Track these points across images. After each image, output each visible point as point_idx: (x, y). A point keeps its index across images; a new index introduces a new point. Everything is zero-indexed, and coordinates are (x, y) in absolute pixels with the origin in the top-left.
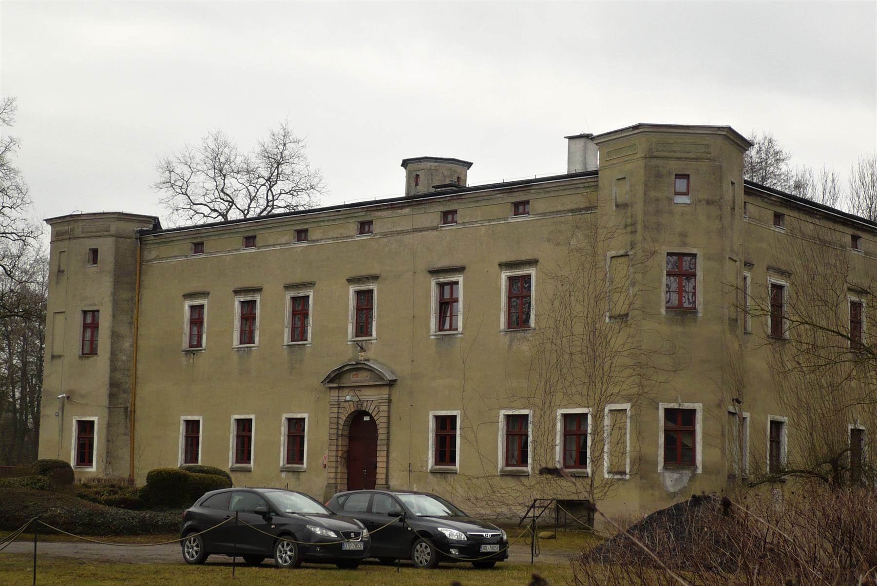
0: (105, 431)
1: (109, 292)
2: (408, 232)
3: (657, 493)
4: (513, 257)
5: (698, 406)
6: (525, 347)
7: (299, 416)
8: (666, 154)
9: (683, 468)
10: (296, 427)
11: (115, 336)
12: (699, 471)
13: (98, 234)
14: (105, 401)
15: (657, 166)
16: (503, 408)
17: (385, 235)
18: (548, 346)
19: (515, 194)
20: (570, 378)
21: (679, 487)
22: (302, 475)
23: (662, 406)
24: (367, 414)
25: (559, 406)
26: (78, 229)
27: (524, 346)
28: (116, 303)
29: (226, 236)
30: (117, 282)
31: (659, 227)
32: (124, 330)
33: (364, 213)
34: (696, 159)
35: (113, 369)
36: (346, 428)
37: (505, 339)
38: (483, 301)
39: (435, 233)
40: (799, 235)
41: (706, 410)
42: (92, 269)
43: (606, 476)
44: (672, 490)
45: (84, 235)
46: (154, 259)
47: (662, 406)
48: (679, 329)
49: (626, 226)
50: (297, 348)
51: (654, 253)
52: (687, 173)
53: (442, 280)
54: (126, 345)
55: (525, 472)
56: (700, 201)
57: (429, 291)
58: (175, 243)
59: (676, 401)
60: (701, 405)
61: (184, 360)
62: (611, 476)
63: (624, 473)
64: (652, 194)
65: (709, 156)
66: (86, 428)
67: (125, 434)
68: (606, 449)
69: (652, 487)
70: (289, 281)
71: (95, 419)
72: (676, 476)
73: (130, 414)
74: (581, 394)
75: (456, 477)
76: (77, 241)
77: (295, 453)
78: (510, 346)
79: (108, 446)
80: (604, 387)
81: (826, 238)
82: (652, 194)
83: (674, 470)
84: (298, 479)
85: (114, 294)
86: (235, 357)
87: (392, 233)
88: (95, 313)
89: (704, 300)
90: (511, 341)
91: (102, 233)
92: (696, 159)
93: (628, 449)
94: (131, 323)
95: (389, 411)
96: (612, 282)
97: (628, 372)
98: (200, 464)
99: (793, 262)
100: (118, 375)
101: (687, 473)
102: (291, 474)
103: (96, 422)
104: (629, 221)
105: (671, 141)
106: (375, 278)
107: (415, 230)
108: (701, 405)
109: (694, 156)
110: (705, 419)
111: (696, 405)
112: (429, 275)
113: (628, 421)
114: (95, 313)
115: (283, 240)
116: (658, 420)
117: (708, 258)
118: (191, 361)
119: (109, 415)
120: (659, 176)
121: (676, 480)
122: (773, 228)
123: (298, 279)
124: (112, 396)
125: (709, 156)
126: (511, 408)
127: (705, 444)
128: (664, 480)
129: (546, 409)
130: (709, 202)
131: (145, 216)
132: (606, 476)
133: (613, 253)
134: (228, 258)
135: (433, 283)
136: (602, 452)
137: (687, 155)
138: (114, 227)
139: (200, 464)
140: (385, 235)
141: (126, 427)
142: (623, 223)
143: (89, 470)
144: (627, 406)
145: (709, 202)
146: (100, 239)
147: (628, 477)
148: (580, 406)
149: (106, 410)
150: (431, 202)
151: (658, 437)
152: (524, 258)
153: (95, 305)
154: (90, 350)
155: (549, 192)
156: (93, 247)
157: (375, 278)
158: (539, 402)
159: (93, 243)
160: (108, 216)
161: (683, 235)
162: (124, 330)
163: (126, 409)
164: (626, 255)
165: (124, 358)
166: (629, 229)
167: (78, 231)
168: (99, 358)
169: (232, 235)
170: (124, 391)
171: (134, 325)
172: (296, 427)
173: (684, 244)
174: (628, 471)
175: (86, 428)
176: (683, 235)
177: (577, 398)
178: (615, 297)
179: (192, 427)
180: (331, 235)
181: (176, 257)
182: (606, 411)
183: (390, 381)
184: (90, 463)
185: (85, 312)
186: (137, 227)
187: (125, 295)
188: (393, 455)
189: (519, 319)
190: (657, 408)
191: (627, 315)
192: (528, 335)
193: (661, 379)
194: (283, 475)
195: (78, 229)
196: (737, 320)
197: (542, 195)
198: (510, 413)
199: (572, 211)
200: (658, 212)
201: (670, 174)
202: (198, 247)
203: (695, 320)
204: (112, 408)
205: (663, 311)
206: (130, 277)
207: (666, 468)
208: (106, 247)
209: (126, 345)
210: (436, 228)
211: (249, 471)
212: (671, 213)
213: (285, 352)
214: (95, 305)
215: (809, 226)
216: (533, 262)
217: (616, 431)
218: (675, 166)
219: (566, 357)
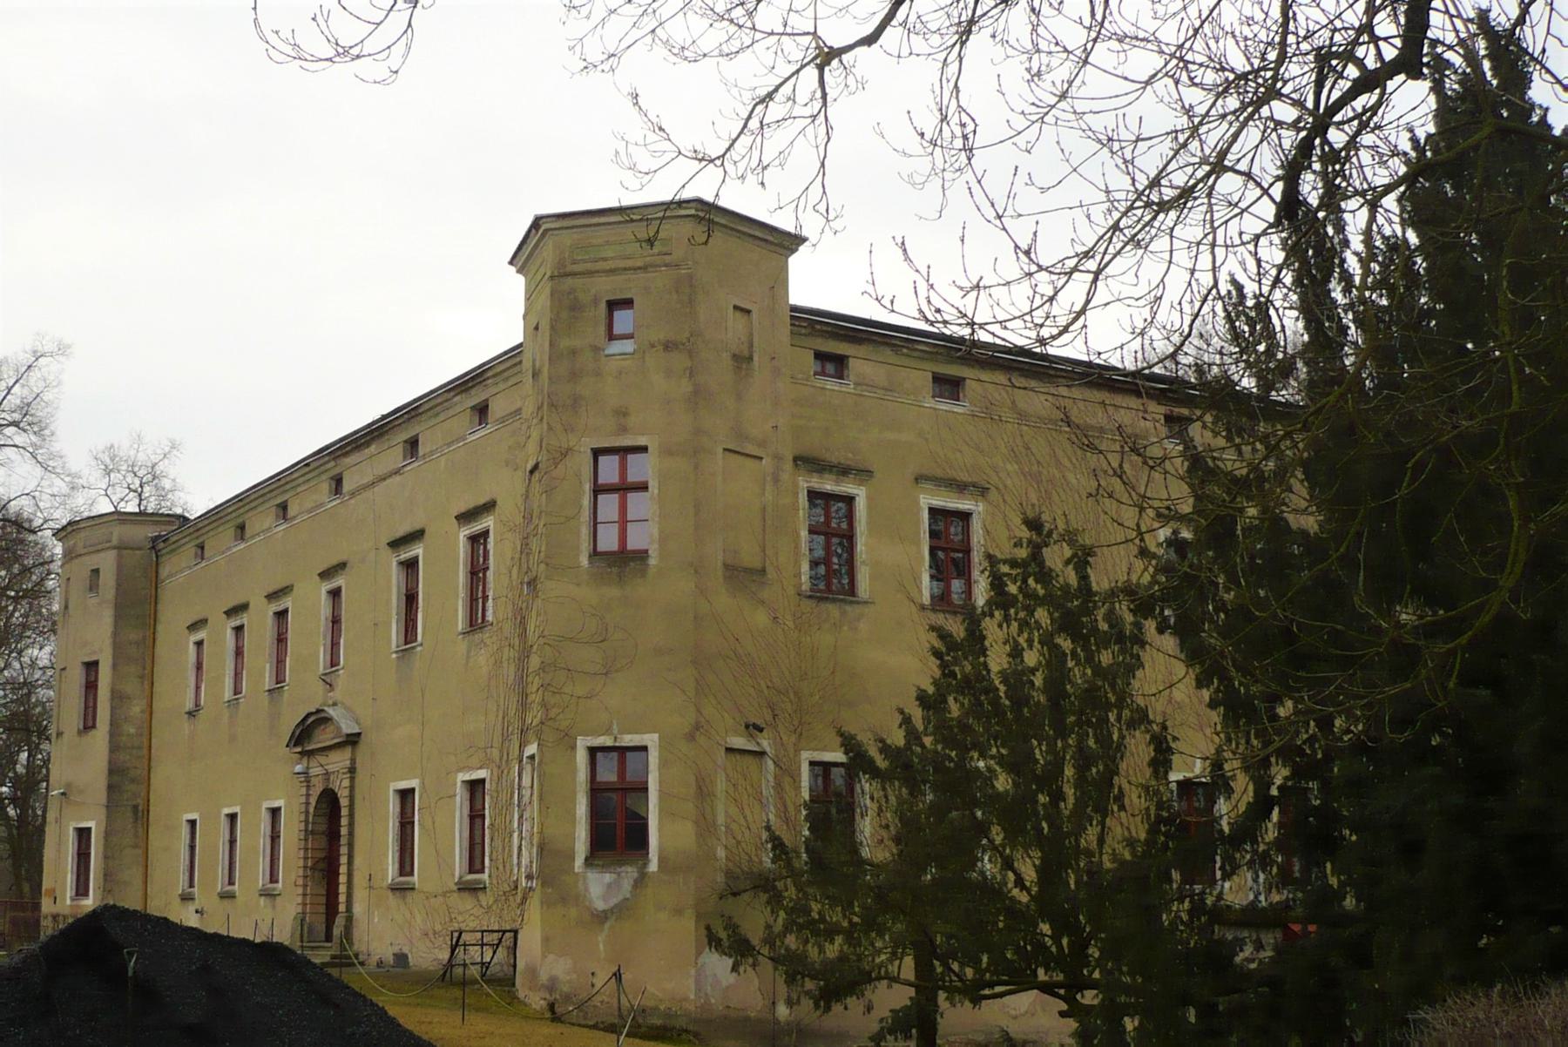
0: (102, 842)
3: (573, 912)
8: (589, 266)
9: (621, 863)
11: (118, 697)
12: (653, 866)
14: (101, 796)
15: (572, 291)
16: (460, 770)
19: (473, 392)
21: (614, 901)
23: (582, 743)
24: (831, 810)
28: (118, 647)
30: (119, 617)
31: (576, 402)
32: (131, 687)
33: (332, 464)
34: (644, 268)
35: (114, 748)
36: (319, 820)
37: (462, 646)
39: (397, 478)
40: (1007, 415)
41: (665, 746)
42: (93, 601)
44: (600, 905)
47: (582, 743)
48: (613, 592)
51: (566, 453)
52: (629, 296)
54: (136, 709)
55: (479, 881)
56: (653, 346)
59: (608, 732)
60: (656, 736)
64: (565, 343)
65: (667, 259)
67: (136, 846)
69: (563, 900)
72: (608, 877)
73: (142, 814)
75: (414, 894)
79: (106, 864)
81: (1093, 422)
82: (565, 343)
83: (604, 867)
85: (115, 634)
88: (96, 663)
89: (661, 532)
92: (644, 268)
94: (142, 677)
99: (995, 469)
100: (123, 757)
101: (630, 872)
105: (600, 241)
108: (656, 736)
109: (639, 263)
110: (664, 764)
111: (646, 736)
114: (96, 663)
116: (574, 771)
117: (667, 452)
119: (108, 817)
120: (576, 308)
121: (609, 886)
122: (930, 403)
124: (111, 788)
125: (667, 259)
127: (664, 812)
128: (587, 889)
130: (668, 346)
137: (629, 263)
138: (118, 533)
141: (136, 836)
145: (668, 346)
146: (102, 555)
149: (104, 811)
151: (573, 801)
154: (89, 725)
155: (507, 379)
161: (622, 413)
162: (131, 687)
163: (135, 807)
165: (132, 731)
170: (133, 781)
171: (148, 678)
173: (623, 430)
175: (83, 834)
176: (622, 413)
183: (348, 735)
184: (86, 894)
186: (152, 532)
187: (134, 635)
188: (358, 861)
190: (574, 748)
193: (580, 690)
196: (763, 571)
197: (502, 386)
200: (574, 376)
201: (596, 301)
203: (643, 573)
204: (111, 806)
205: (584, 561)
206: (138, 606)
207: (589, 862)
208: (107, 562)
209: (136, 709)
210: (397, 472)
212: (598, 374)
215: (1038, 400)
218: (608, 287)
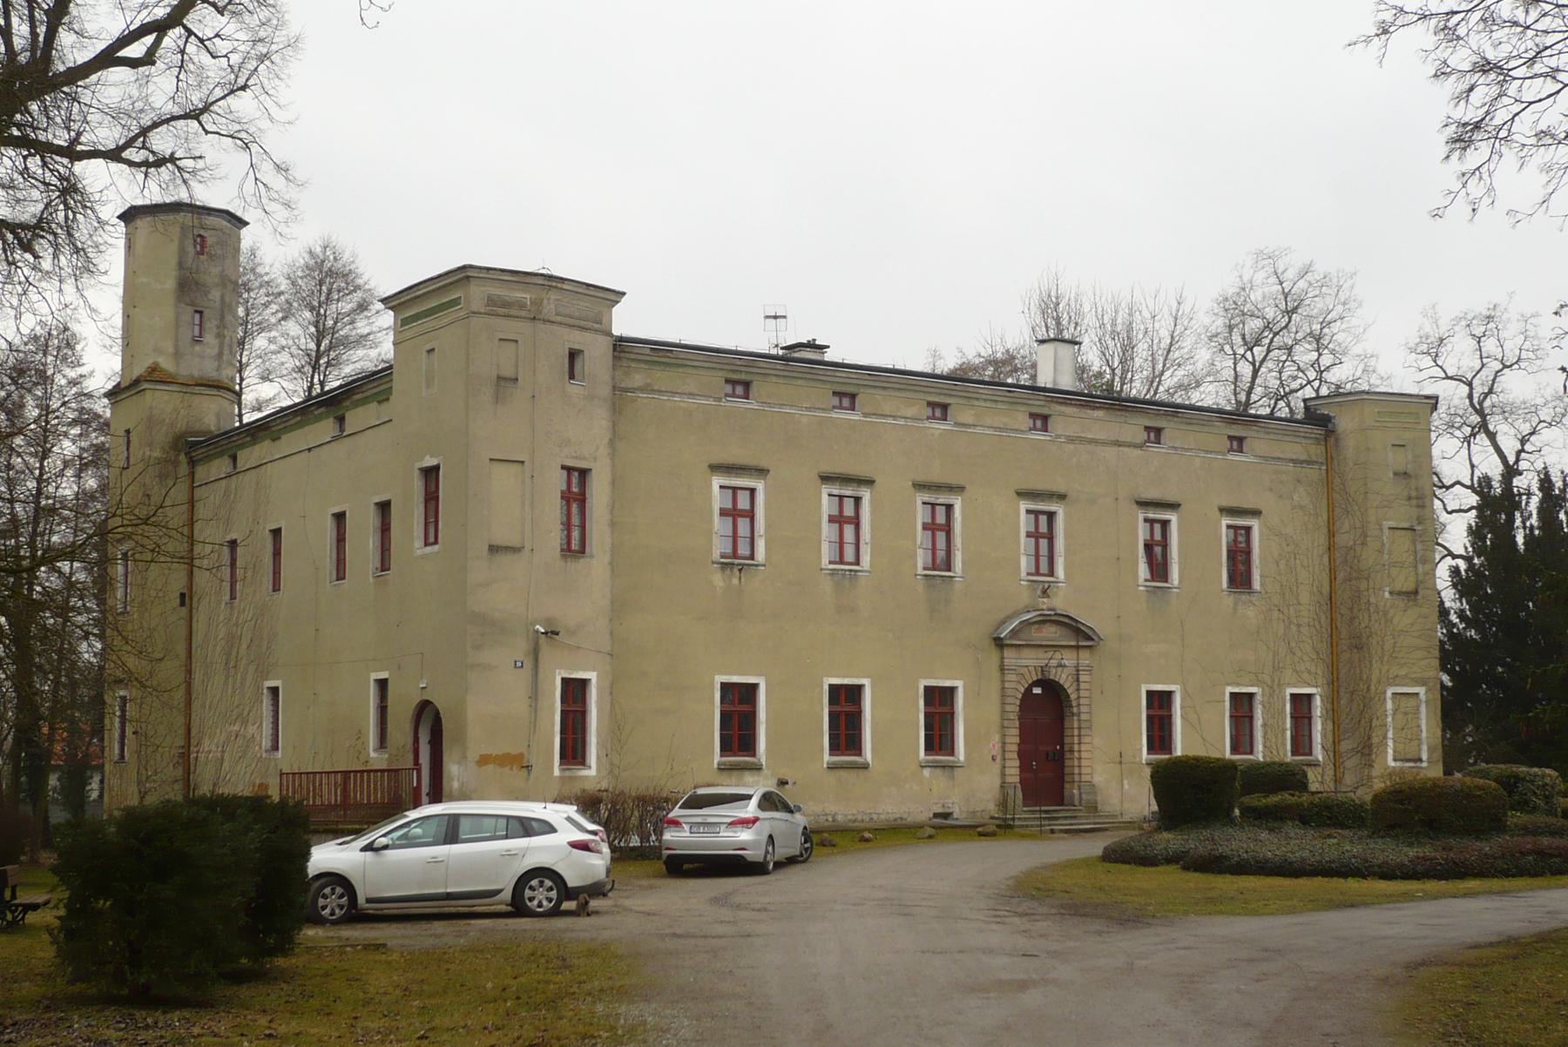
1: (606, 441)
2: (1104, 443)
4: (1234, 504)
5: (865, 682)
6: (1251, 612)
7: (948, 683)
10: (939, 701)
13: (583, 323)
17: (1071, 440)
18: (1276, 613)
20: (1299, 654)
22: (958, 772)
25: (1289, 685)
26: (551, 303)
27: (1251, 612)
29: (800, 382)
37: (1228, 600)
38: (1196, 549)
43: (1392, 764)
45: (559, 319)
46: (642, 389)
49: (1410, 498)
50: (939, 581)
53: (1151, 516)
57: (1136, 529)
58: (690, 371)
61: (718, 579)
62: (1399, 764)
63: (1420, 760)
66: (575, 691)
68: (1390, 735)
70: (921, 478)
71: (592, 676)
74: (1309, 672)
76: (548, 326)
77: (939, 736)
78: (1235, 609)
80: (1385, 669)
84: (952, 778)
86: (827, 585)
87: (1082, 440)
90: (1236, 604)
91: (590, 324)
93: (1424, 735)
95: (1003, 682)
96: (1390, 554)
97: (1420, 654)
98: (1178, 751)
102: (938, 771)
103: (594, 681)
104: (1414, 494)
106: (1062, 497)
107: (1118, 444)
112: (1135, 506)
113: (1423, 709)
114: (584, 473)
115: (910, 412)
118: (735, 581)
123: (936, 476)
126: (1238, 685)
129: (1273, 689)
131: (440, 276)
132: (1392, 764)
133: (1393, 524)
134: (804, 420)
135: (1141, 517)
136: (1385, 737)
139: (1178, 751)
140: (1071, 440)
142: (1405, 494)
143: (585, 773)
144: (1421, 690)
147: (1425, 765)
148: (1309, 685)
150: (1142, 411)
152: (1245, 506)
153: (585, 459)
156: (576, 347)
157: (1062, 497)
158: (1268, 679)
159: (577, 339)
160: (528, 279)
164: (1412, 529)
166: (1414, 502)
167: (549, 308)
168: (594, 561)
169: (812, 384)
172: (939, 701)
174: (1425, 757)
177: (1306, 676)
178: (1394, 572)
179: (382, 684)
180: (989, 422)
181: (691, 395)
182: (1389, 694)
185: (569, 470)
189: (1240, 578)
191: (1416, 592)
192: (1254, 598)
194: (926, 772)
195: (551, 303)
198: (1236, 690)
199: (1292, 461)
202: (1042, 421)
211: (865, 767)
213: (920, 585)
214: (585, 459)
216: (1255, 513)
217: (1400, 716)
219: (1294, 628)
